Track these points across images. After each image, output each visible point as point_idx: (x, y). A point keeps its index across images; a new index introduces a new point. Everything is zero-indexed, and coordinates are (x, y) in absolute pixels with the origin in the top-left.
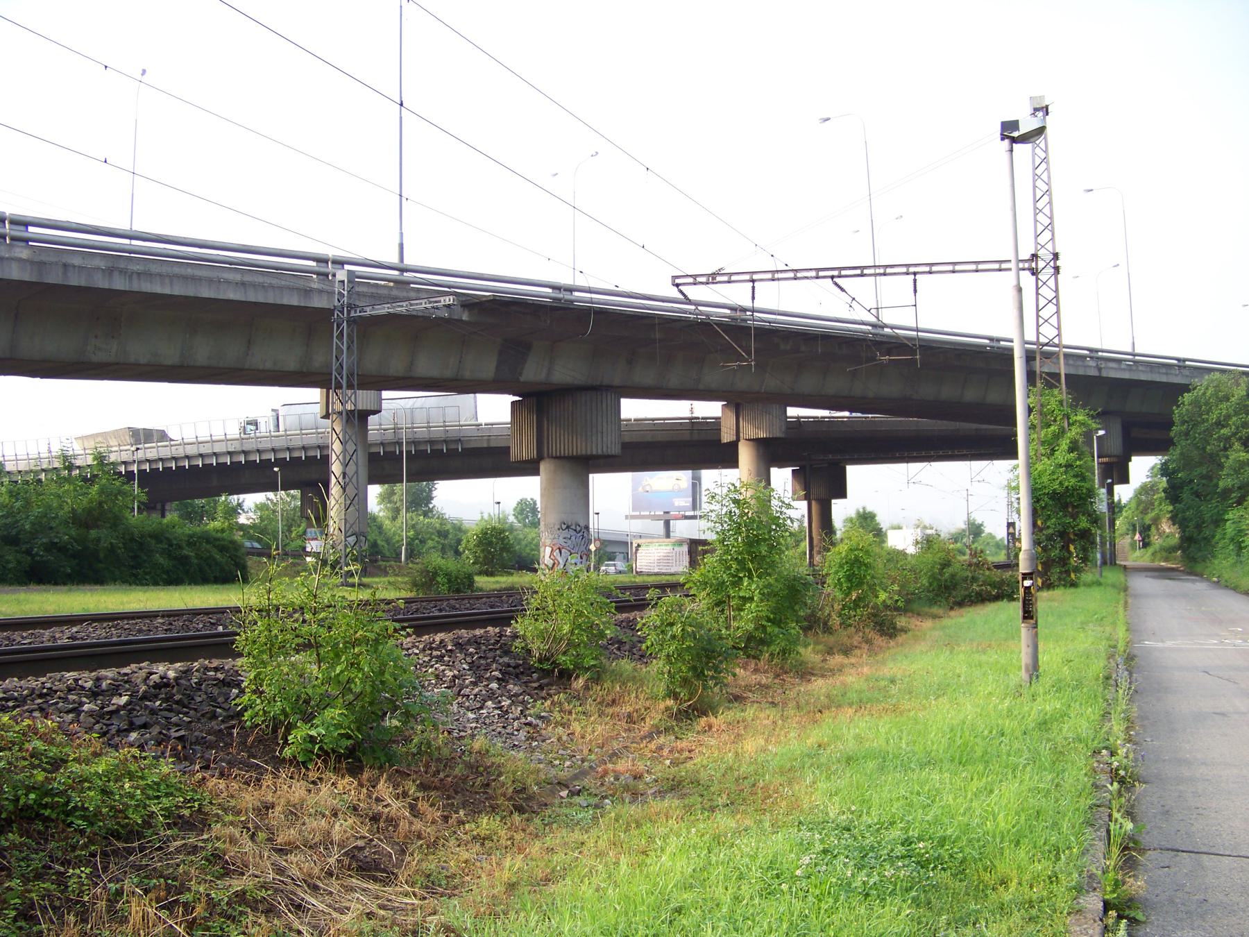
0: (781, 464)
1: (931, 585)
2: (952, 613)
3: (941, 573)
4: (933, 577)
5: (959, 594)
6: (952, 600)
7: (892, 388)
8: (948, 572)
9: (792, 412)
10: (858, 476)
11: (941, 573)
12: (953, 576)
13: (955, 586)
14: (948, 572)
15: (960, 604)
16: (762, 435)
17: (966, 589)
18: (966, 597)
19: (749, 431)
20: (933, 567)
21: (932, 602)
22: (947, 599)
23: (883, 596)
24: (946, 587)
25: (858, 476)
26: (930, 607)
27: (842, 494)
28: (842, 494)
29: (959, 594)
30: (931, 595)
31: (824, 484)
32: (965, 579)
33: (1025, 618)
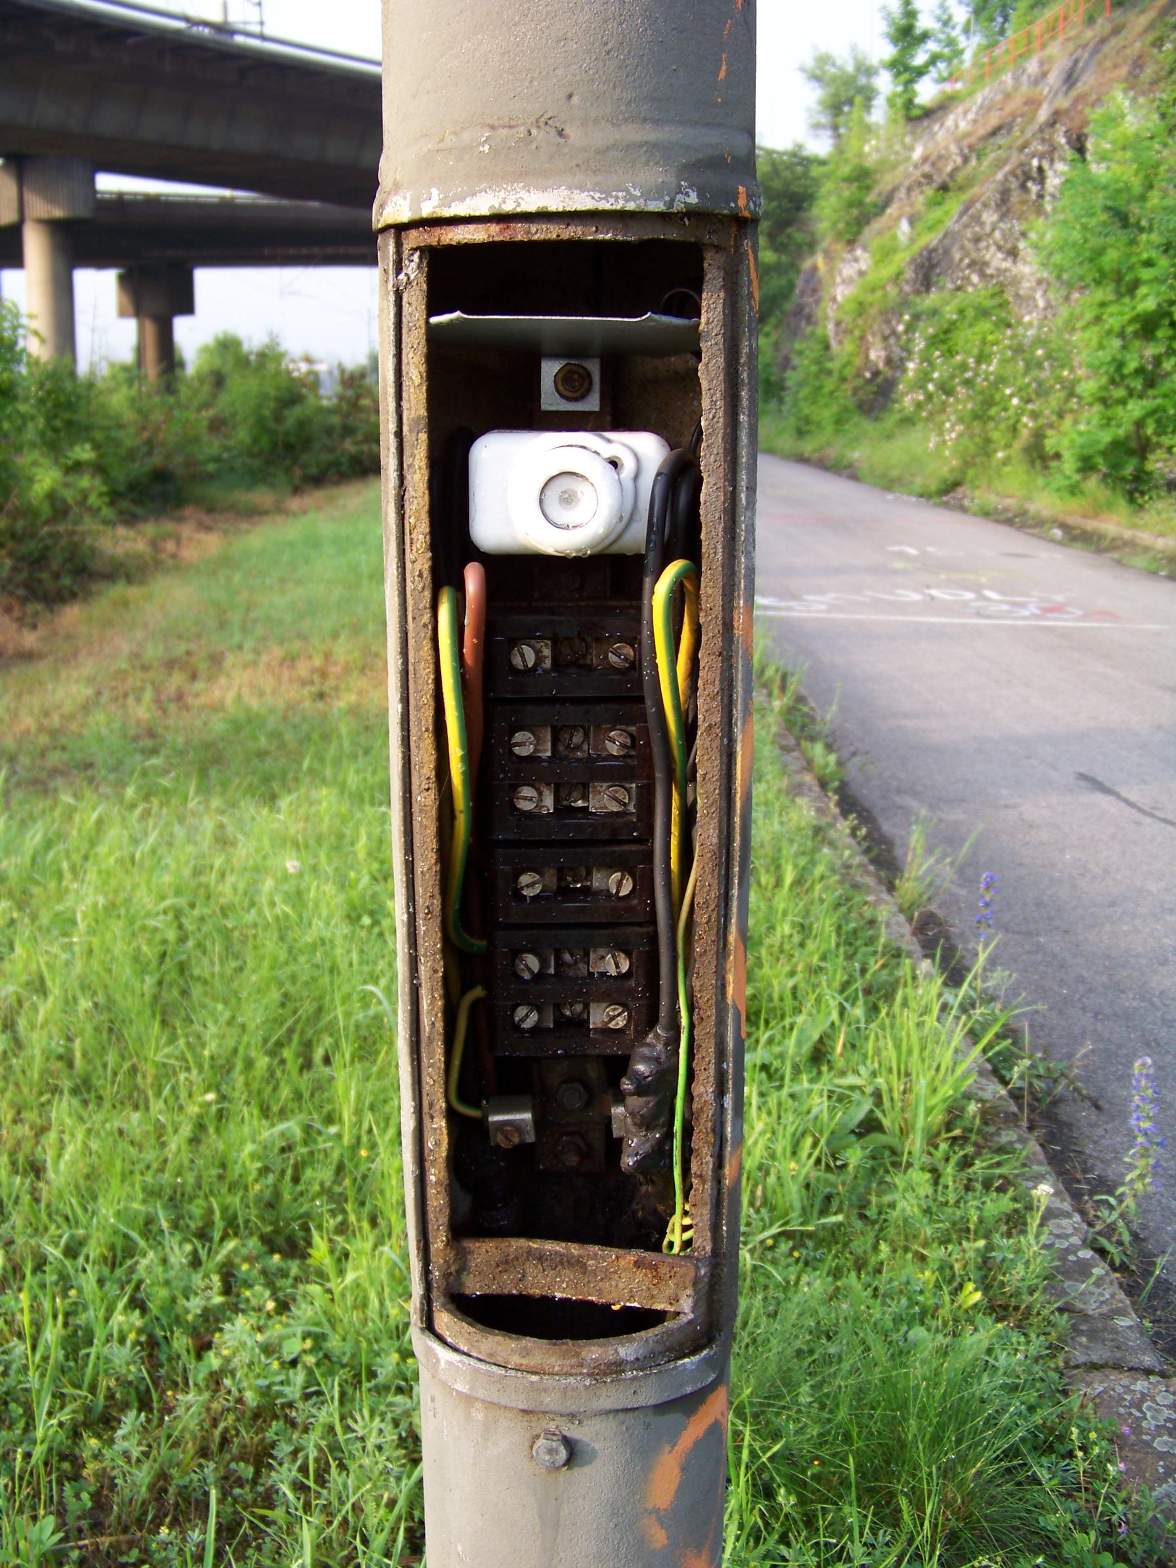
0: (99, 261)
1: (256, 441)
2: (294, 504)
3: (278, 418)
4: (261, 423)
5: (314, 460)
6: (298, 472)
7: (249, 137)
8: (293, 415)
9: (108, 183)
10: (210, 283)
11: (278, 418)
12: (302, 424)
13: (306, 443)
14: (293, 415)
15: (318, 480)
16: (58, 213)
17: (331, 450)
18: (330, 465)
19: (39, 207)
20: (260, 406)
21: (256, 478)
22: (288, 470)
23: (1065, 373)
24: (289, 447)
25: (210, 283)
26: (249, 488)
27: (188, 308)
28: (188, 308)
29: (314, 460)
30: (256, 463)
31: (160, 294)
32: (329, 431)
33: (487, 1190)
